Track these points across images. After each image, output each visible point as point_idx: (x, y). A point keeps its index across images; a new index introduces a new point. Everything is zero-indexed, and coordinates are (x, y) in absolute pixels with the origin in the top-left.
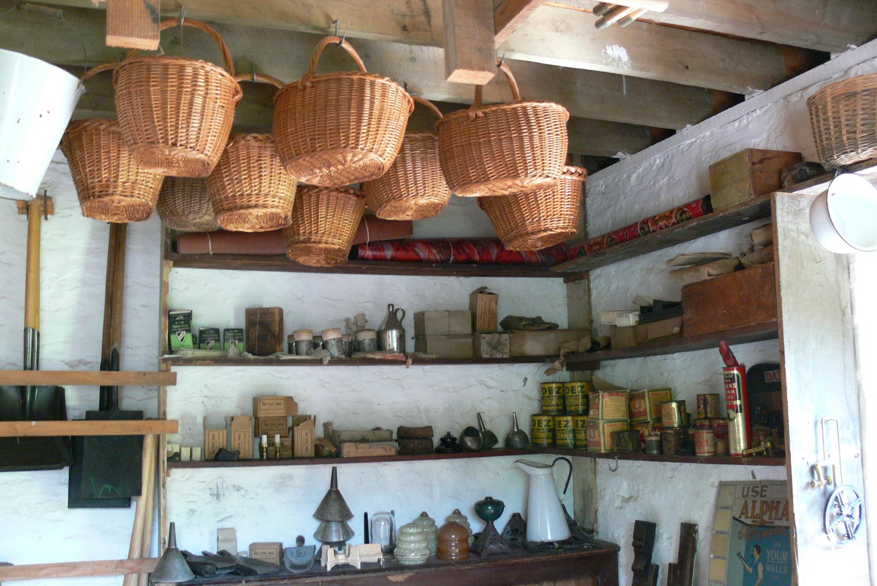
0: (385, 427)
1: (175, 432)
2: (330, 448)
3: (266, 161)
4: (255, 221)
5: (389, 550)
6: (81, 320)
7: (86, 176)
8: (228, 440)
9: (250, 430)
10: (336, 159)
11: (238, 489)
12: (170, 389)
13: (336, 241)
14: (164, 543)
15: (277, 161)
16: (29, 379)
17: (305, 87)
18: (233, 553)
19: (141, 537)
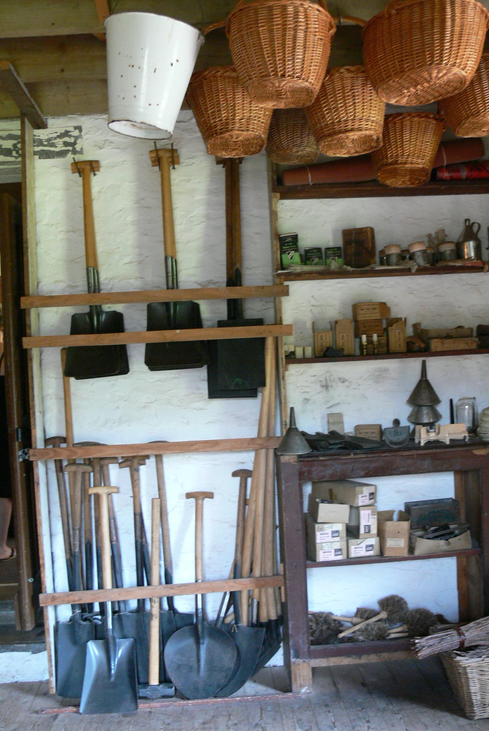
0: (466, 326)
1: (290, 334)
2: (421, 344)
3: (358, 90)
4: (351, 145)
5: (473, 430)
6: (208, 248)
7: (209, 117)
8: (334, 340)
9: (352, 331)
10: (422, 77)
11: (343, 381)
12: (284, 299)
13: (420, 161)
14: (286, 425)
15: (369, 87)
16: (171, 296)
17: (390, 16)
18: (341, 433)
19: (266, 420)
